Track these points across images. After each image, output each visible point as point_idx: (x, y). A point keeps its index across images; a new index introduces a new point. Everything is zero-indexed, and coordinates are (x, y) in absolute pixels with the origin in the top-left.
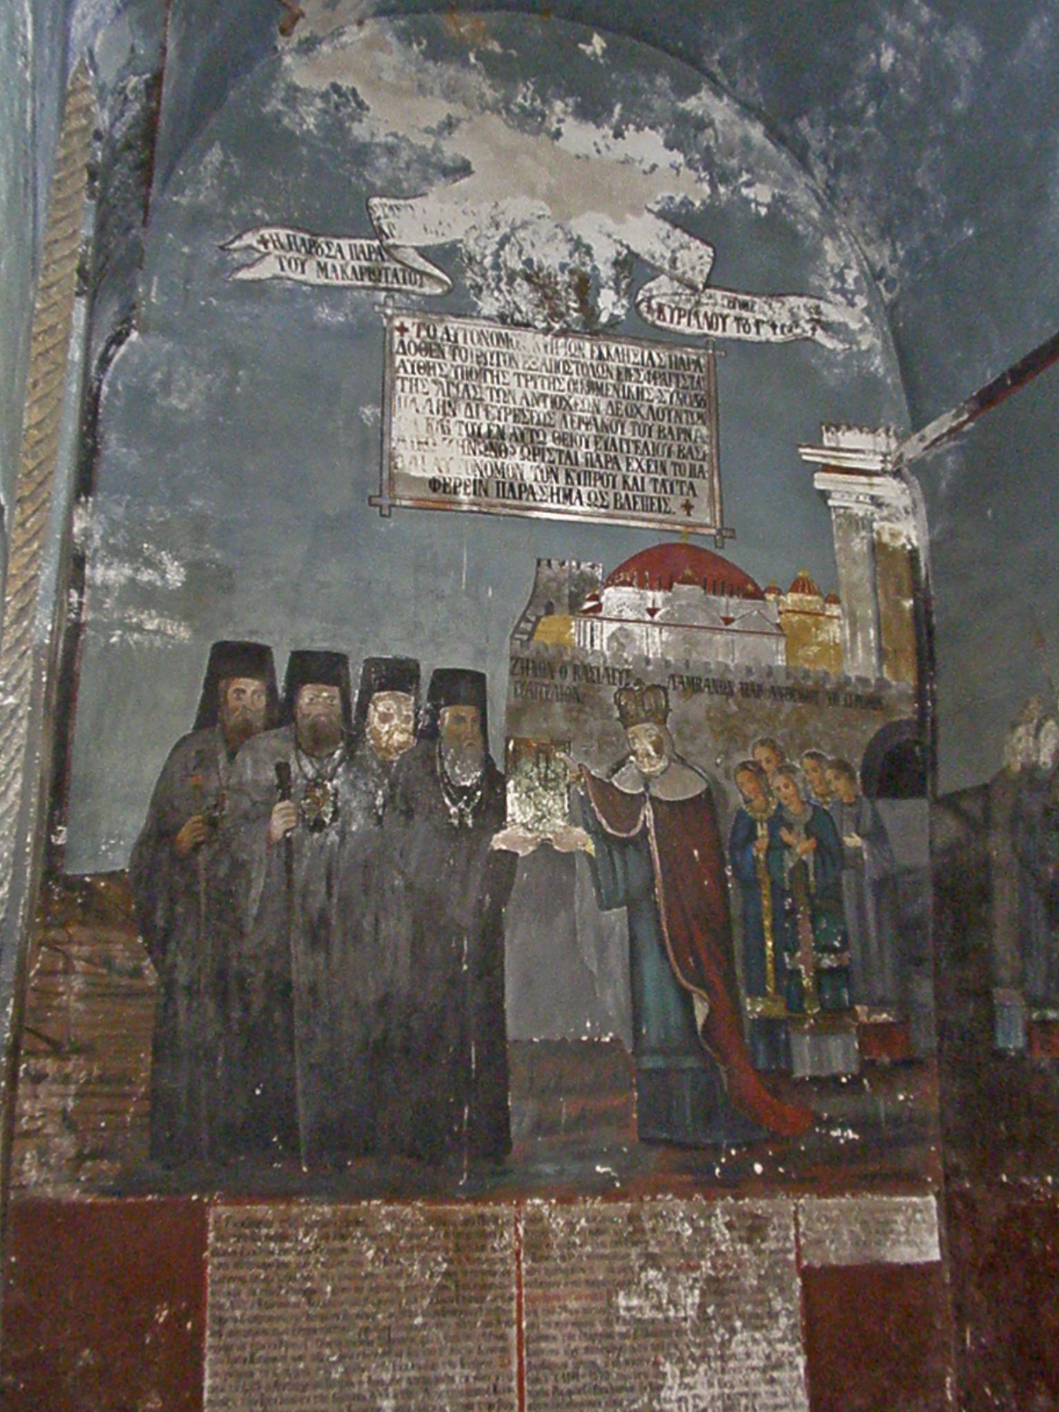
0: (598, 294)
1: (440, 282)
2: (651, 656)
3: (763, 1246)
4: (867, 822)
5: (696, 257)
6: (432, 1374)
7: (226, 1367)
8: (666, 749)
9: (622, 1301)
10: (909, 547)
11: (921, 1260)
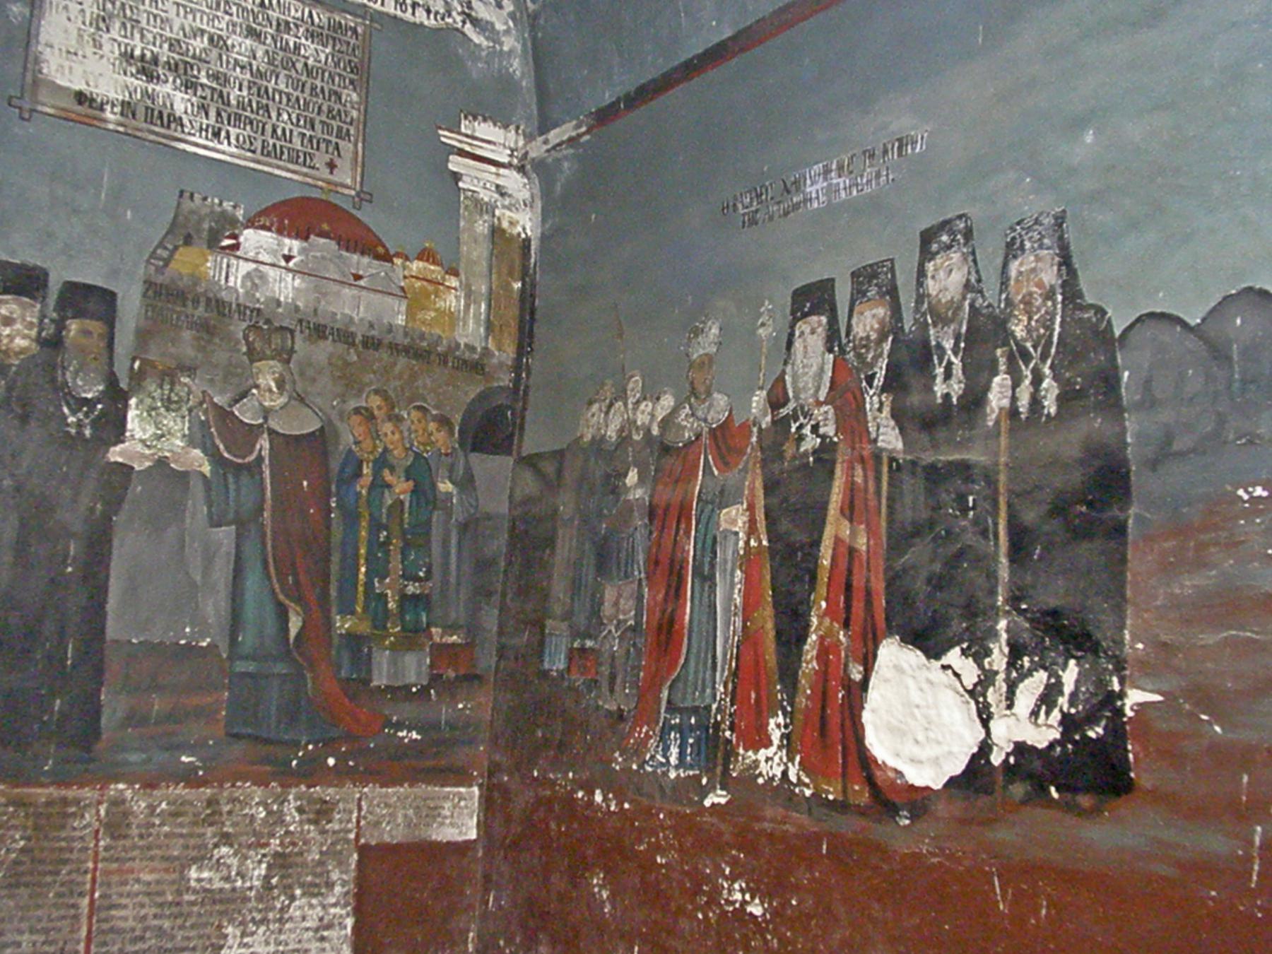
2: (282, 299)
10: (523, 236)
11: (460, 839)
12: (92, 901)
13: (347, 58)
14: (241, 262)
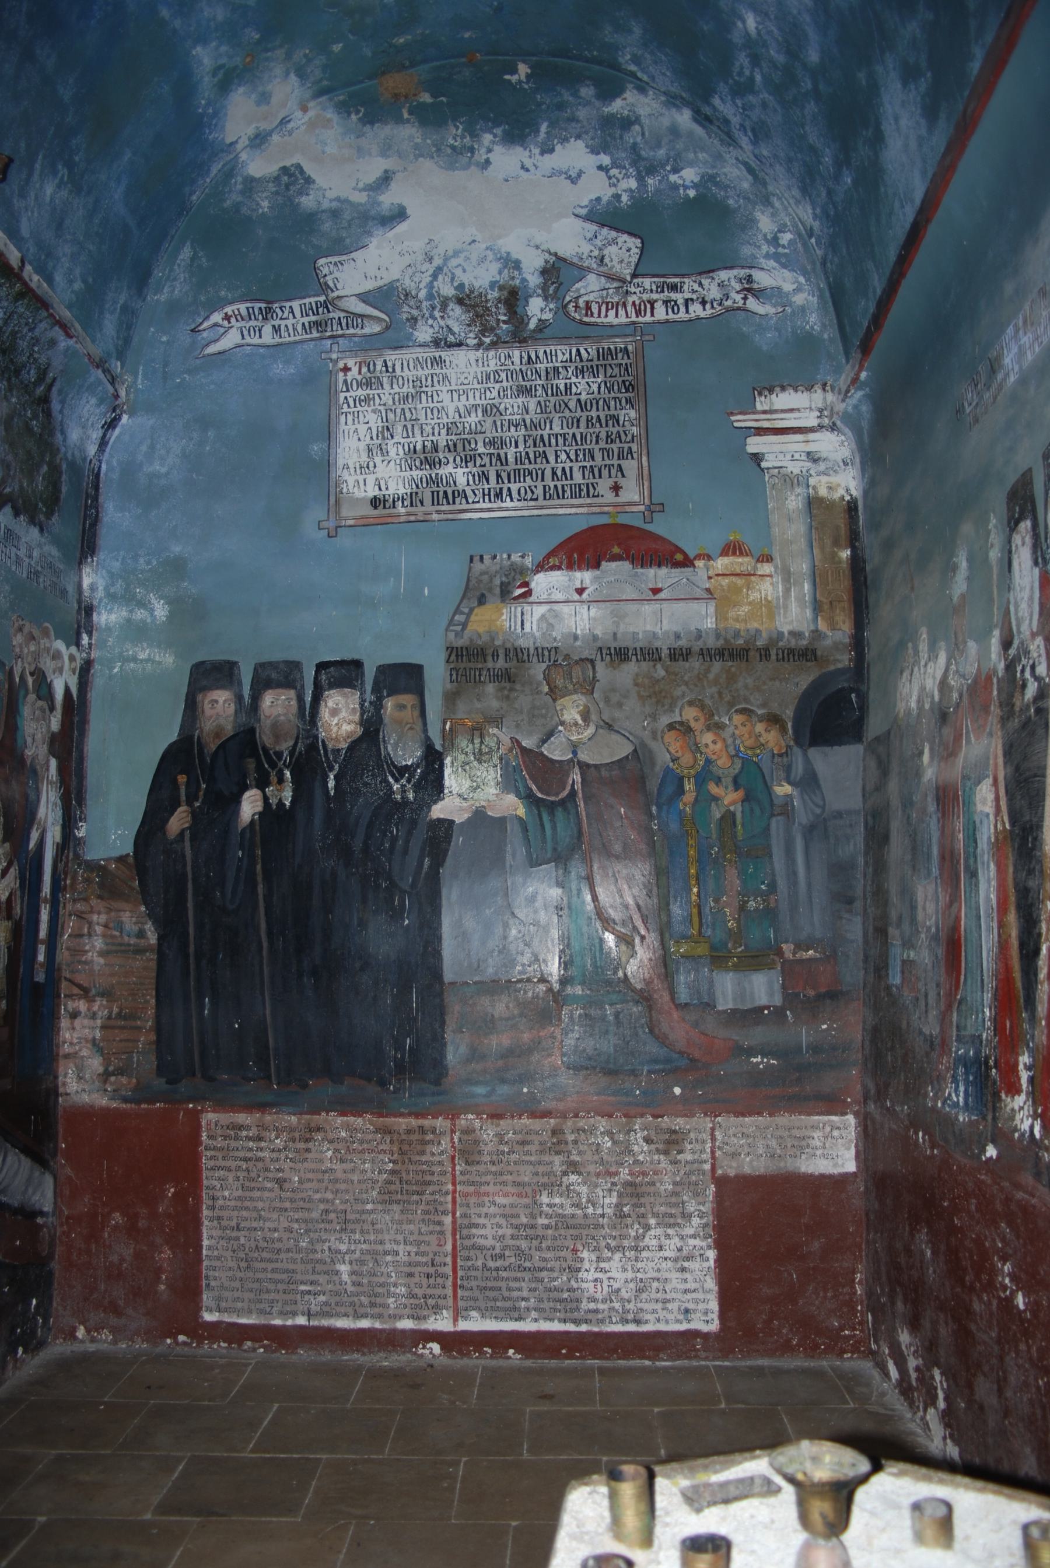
0: (527, 304)
1: (378, 320)
2: (579, 632)
3: (679, 1157)
4: (799, 769)
5: (622, 252)
6: (380, 1248)
7: (219, 1233)
8: (594, 717)
9: (545, 1199)
10: (847, 498)
11: (836, 1171)
12: (454, 1222)
13: (620, 380)
14: (535, 607)
